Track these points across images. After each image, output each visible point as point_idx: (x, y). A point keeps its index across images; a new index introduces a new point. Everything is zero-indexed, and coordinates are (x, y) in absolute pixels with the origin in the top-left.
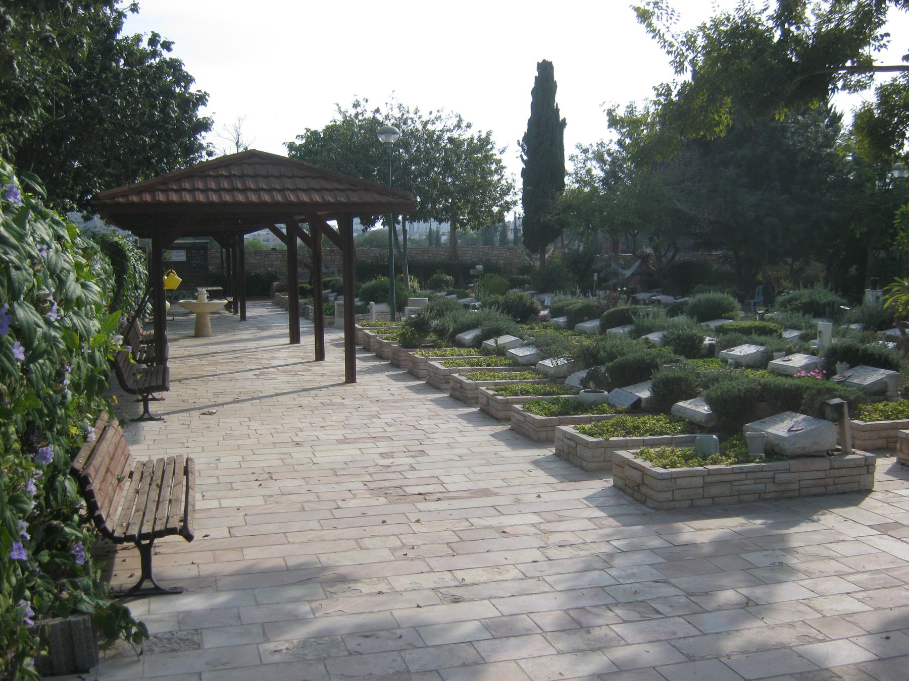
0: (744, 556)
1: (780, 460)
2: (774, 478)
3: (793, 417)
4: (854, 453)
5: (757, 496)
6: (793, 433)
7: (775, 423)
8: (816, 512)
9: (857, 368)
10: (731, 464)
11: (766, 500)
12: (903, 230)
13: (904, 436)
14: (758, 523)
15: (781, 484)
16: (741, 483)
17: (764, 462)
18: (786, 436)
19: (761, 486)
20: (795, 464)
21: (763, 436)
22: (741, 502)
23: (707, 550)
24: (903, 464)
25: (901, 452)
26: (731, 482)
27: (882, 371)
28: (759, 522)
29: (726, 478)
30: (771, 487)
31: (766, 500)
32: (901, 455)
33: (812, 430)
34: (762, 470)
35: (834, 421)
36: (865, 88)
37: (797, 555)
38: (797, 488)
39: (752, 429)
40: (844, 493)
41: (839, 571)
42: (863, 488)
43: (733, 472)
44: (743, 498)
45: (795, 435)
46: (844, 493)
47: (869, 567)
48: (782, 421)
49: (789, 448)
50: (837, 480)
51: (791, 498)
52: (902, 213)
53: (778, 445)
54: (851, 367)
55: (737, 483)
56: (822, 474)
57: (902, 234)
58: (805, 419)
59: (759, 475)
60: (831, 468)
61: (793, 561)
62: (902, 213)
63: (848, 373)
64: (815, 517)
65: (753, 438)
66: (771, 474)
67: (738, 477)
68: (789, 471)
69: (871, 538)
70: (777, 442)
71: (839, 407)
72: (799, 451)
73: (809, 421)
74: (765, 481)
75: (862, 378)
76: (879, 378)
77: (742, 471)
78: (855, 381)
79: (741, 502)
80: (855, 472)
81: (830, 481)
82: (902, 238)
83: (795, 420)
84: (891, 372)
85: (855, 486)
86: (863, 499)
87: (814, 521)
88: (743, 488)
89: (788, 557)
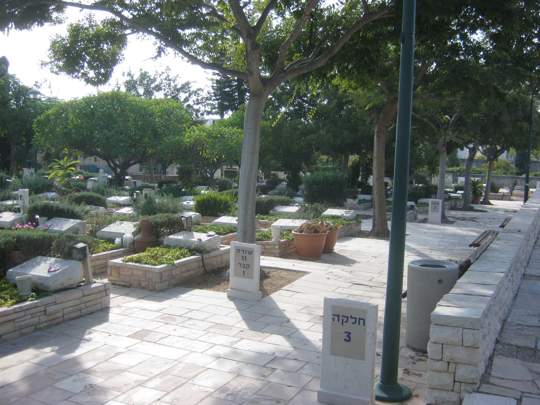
0: (57, 385)
1: (47, 295)
2: (45, 311)
3: (46, 260)
4: (95, 282)
5: (33, 327)
6: (53, 273)
7: (34, 267)
8: (84, 333)
9: (53, 219)
10: (12, 305)
11: (41, 329)
12: (38, 132)
13: (113, 264)
14: (48, 352)
15: (51, 314)
16: (22, 319)
17: (36, 299)
18: (49, 276)
19: (36, 319)
20: (58, 297)
21: (30, 279)
22: (22, 335)
23: (23, 388)
24: (113, 284)
25: (111, 275)
26: (14, 320)
27: (72, 220)
28: (48, 350)
29: (10, 317)
30: (43, 318)
31: (41, 329)
32: (111, 278)
33: (67, 269)
34: (36, 306)
35: (80, 260)
36: (62, 23)
37: (97, 374)
38: (62, 315)
39: (16, 273)
40: (92, 313)
41: (139, 381)
42: (103, 307)
43: (15, 312)
44: (24, 331)
45: (55, 275)
46: (92, 313)
47: (156, 372)
48: (38, 264)
49: (53, 286)
50: (88, 304)
51: (58, 324)
52: (38, 120)
53: (42, 284)
54: (48, 220)
55: (18, 320)
56: (77, 302)
57: (37, 134)
58: (56, 262)
59: (35, 310)
60: (83, 296)
61: (98, 380)
62: (38, 120)
63: (49, 223)
64: (87, 337)
65: (21, 281)
66: (43, 308)
67: (19, 315)
68: (55, 303)
69: (136, 346)
70: (41, 282)
71: (84, 249)
72: (59, 287)
73: (60, 262)
74: (39, 314)
75: (60, 226)
76: (72, 225)
77: (22, 310)
78: (56, 229)
79: (22, 335)
80: (98, 296)
81: (83, 306)
82: (37, 136)
83: (48, 262)
84: (78, 221)
85: (99, 307)
86: (108, 316)
87: (88, 341)
88: (23, 323)
89: (92, 377)
